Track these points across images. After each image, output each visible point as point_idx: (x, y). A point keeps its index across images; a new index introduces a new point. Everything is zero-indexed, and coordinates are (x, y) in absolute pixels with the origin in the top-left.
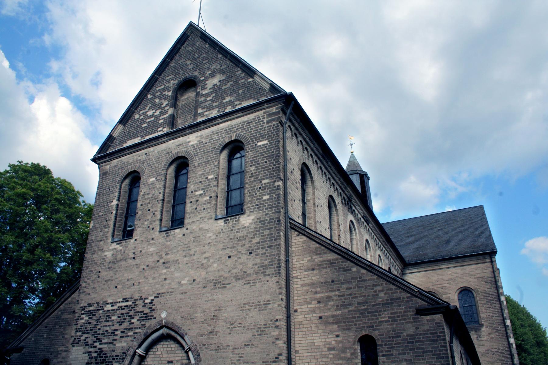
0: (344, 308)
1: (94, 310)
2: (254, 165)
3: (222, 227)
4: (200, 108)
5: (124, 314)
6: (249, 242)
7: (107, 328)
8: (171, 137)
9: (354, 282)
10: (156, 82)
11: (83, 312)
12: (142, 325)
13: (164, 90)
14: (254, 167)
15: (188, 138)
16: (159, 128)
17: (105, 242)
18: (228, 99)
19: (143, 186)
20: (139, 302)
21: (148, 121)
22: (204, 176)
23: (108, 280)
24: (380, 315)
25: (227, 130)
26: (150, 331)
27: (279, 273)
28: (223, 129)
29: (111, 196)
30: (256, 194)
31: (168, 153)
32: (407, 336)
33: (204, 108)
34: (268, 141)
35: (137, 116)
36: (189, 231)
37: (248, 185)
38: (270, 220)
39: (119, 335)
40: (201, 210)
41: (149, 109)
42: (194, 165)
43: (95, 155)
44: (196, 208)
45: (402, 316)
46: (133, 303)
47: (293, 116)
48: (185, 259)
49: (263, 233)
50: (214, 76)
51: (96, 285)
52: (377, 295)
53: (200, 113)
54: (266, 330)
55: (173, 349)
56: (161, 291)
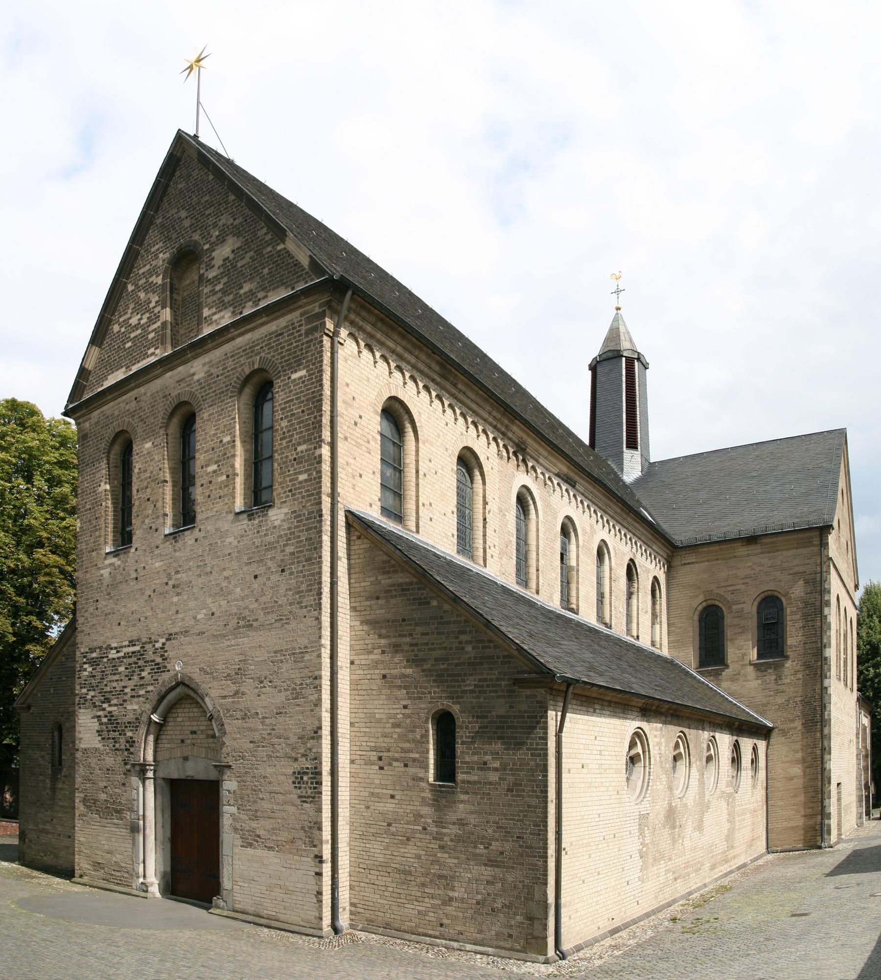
2: (286, 417)
3: (245, 526)
4: (206, 306)
5: (131, 664)
7: (115, 684)
8: (167, 367)
9: (433, 624)
10: (136, 258)
11: (85, 660)
12: (154, 680)
13: (150, 273)
14: (286, 420)
15: (192, 367)
16: (149, 349)
17: (98, 553)
18: (246, 288)
19: (136, 457)
20: (148, 647)
21: (132, 335)
23: (109, 614)
24: (464, 681)
25: (246, 350)
26: (164, 690)
27: (320, 604)
28: (241, 348)
29: (97, 477)
32: (498, 717)
33: (212, 307)
34: (307, 372)
35: (116, 328)
37: (279, 455)
39: (129, 695)
40: (215, 499)
41: (132, 313)
43: (67, 406)
44: (209, 496)
45: (493, 686)
46: (141, 648)
47: (358, 314)
48: (200, 580)
49: (299, 537)
50: (225, 240)
51: (94, 621)
52: (463, 648)
54: (303, 691)
55: (196, 714)
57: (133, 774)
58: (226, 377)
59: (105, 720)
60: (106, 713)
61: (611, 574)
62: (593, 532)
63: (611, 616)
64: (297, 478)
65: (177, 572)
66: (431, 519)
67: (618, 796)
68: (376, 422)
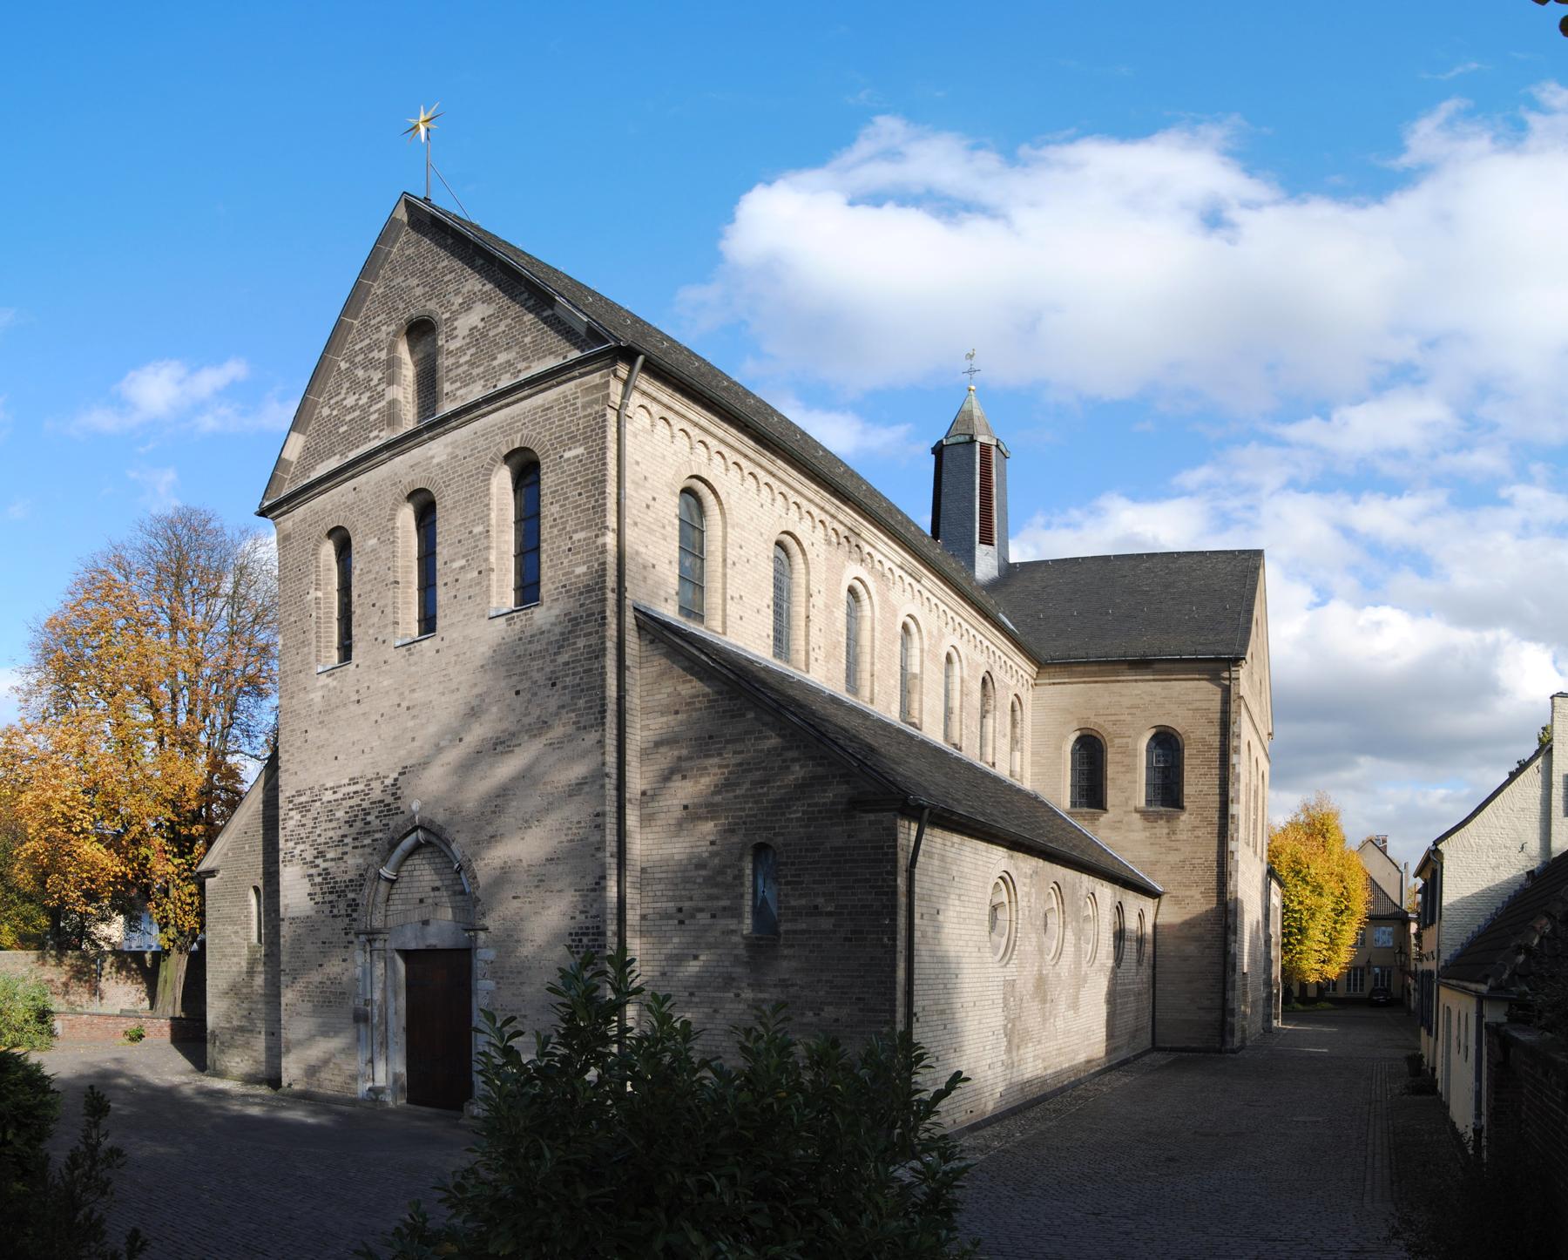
0: (727, 791)
1: (307, 802)
2: (557, 502)
6: (552, 661)
11: (291, 806)
13: (370, 348)
15: (430, 449)
16: (371, 431)
18: (502, 358)
19: (357, 556)
20: (374, 784)
22: (466, 528)
23: (323, 746)
30: (562, 563)
31: (395, 484)
34: (585, 449)
36: (446, 642)
37: (548, 545)
38: (588, 616)
40: (464, 599)
42: (445, 506)
43: (261, 504)
44: (455, 597)
48: (443, 699)
53: (447, 394)
56: (408, 763)
57: (357, 947)
58: (475, 459)
59: (318, 880)
60: (319, 870)
61: (962, 686)
62: (941, 635)
63: (961, 735)
64: (574, 571)
65: (413, 690)
66: (741, 618)
67: (979, 955)
68: (673, 504)
